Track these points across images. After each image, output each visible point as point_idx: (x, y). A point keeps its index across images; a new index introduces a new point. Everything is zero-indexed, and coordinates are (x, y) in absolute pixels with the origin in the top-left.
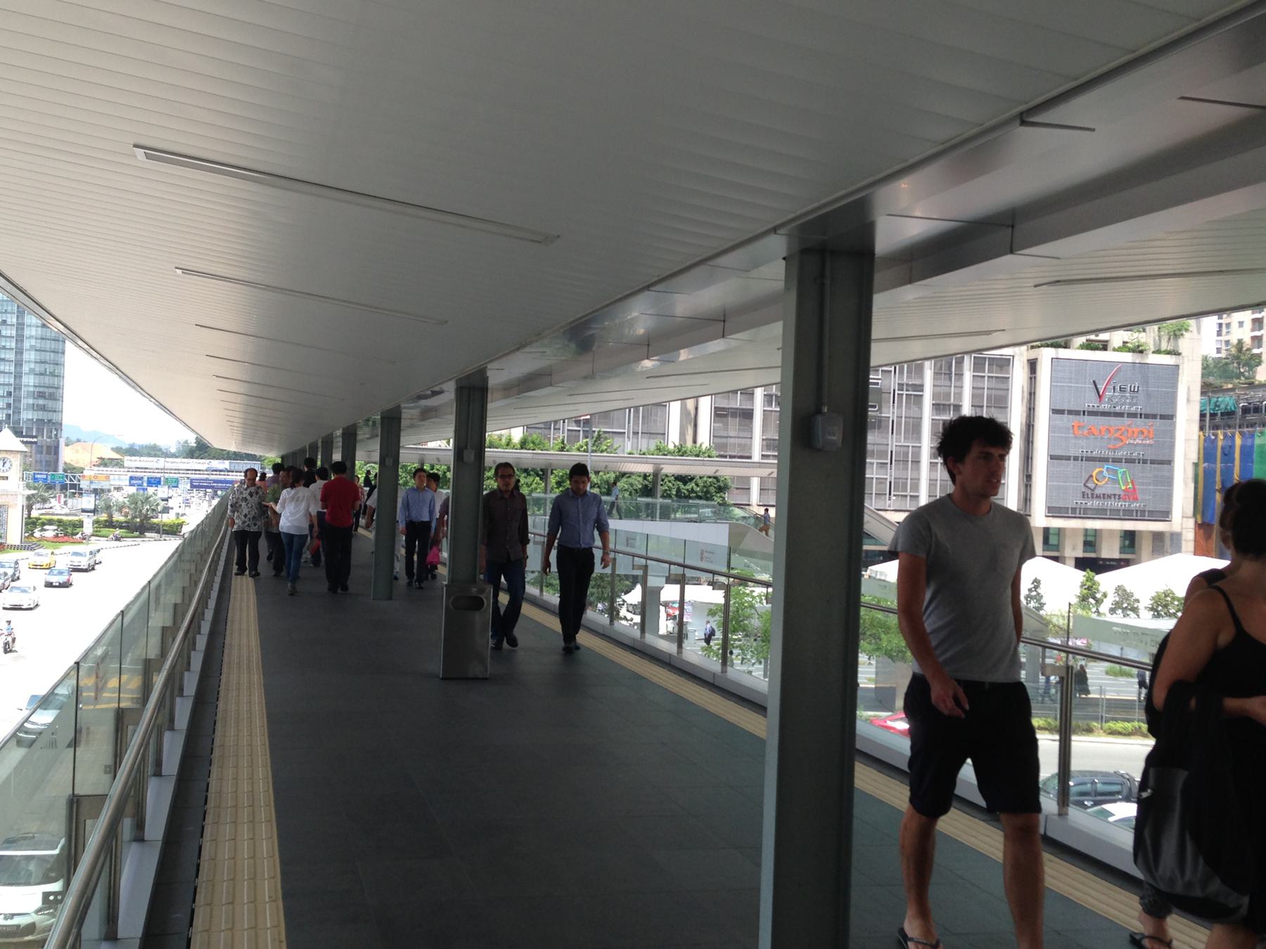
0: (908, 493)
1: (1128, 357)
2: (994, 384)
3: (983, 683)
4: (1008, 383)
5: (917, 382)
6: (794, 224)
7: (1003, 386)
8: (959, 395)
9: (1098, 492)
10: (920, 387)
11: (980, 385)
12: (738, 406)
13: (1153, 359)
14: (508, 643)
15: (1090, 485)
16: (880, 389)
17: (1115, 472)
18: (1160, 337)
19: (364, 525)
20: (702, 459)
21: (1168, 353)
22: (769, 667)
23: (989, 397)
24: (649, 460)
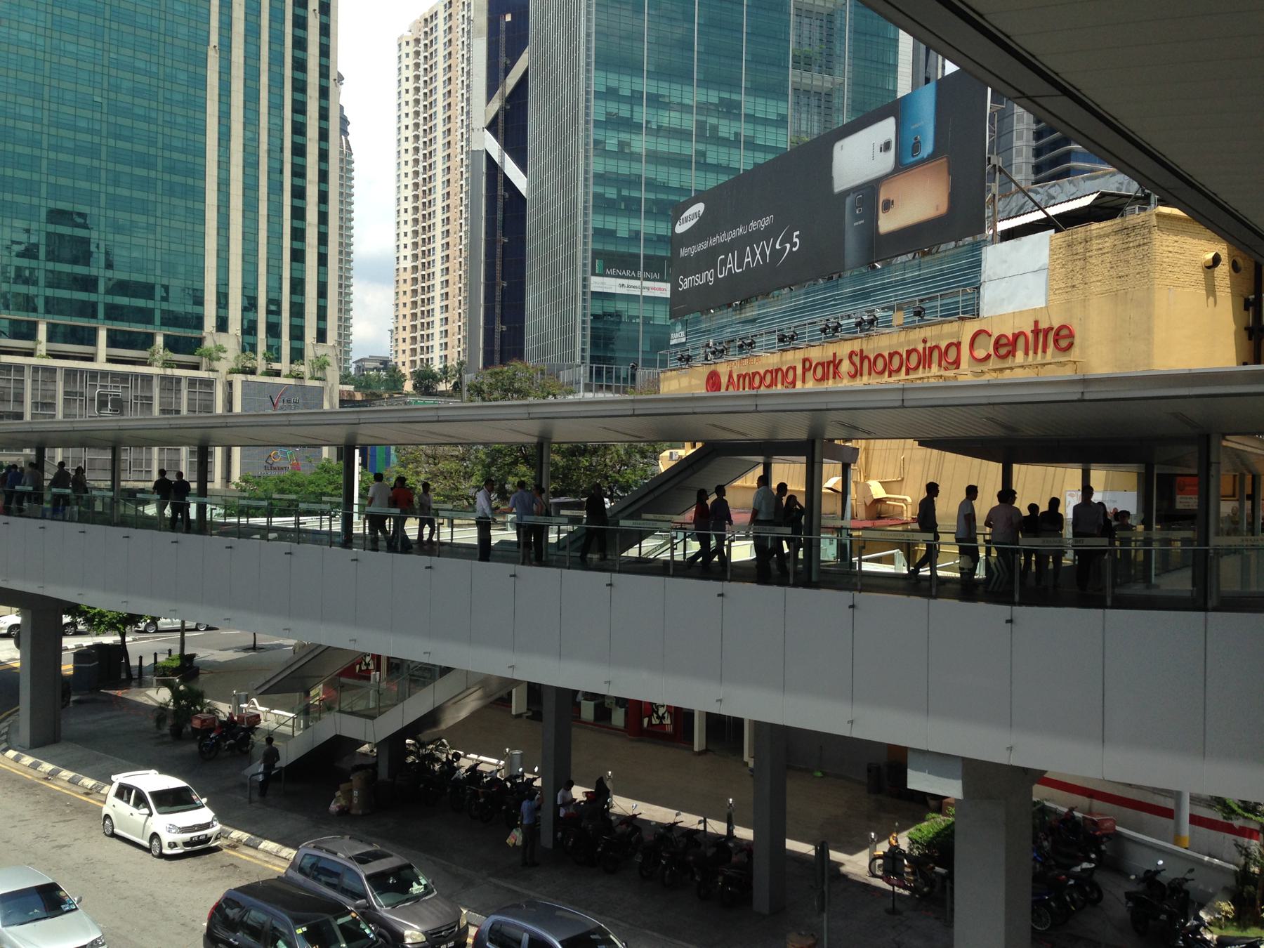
0: (144, 469)
1: (292, 381)
2: (203, 397)
3: (929, 773)
4: (212, 396)
5: (148, 395)
6: (590, 211)
7: (210, 398)
8: (179, 404)
9: (275, 466)
10: (151, 398)
11: (192, 397)
12: (11, 410)
13: (309, 383)
14: (852, 849)
15: (270, 462)
16: (121, 399)
17: (286, 453)
18: (313, 368)
19: (195, 492)
20: (631, 397)
21: (318, 379)
22: (1206, 858)
23: (200, 405)
24: (292, 418)
